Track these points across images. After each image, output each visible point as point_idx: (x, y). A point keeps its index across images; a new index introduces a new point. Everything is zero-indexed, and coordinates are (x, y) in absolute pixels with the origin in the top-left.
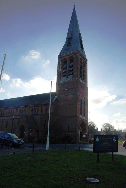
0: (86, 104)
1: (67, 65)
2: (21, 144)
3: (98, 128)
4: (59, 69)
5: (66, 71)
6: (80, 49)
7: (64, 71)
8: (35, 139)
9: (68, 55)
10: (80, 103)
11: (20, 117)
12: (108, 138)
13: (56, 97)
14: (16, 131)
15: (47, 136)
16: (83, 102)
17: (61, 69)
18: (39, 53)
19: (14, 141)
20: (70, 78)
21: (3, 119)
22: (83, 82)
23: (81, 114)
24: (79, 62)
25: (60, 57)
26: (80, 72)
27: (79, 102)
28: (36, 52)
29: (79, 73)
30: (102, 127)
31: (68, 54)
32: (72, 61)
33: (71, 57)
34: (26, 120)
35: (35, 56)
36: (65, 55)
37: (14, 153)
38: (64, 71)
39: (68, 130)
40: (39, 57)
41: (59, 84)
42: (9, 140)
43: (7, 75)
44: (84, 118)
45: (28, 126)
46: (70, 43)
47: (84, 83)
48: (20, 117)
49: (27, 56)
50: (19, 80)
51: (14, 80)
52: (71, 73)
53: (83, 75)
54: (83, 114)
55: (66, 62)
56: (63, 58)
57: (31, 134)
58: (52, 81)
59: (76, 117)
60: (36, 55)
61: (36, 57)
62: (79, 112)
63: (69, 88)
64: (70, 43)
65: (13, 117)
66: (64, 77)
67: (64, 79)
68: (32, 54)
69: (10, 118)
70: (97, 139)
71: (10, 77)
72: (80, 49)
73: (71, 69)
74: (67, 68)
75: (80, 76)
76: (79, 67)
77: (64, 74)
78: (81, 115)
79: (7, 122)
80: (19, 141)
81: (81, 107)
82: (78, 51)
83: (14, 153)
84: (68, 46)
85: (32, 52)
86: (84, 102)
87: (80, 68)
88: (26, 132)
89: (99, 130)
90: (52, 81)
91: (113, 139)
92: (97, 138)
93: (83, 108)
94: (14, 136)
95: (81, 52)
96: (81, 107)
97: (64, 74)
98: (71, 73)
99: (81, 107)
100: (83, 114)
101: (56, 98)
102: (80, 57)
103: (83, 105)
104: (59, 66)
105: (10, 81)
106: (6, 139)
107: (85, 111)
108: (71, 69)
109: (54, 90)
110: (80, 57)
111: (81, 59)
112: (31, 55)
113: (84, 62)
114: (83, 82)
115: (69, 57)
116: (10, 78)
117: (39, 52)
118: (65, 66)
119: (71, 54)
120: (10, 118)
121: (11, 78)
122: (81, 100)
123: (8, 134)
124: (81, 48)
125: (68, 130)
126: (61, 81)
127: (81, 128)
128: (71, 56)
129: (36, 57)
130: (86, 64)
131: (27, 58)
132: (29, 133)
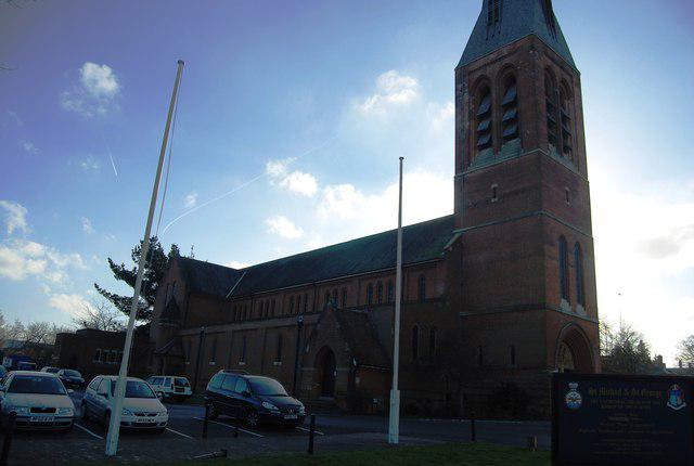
0: (585, 254)
1: (494, 102)
2: (295, 417)
3: (660, 358)
4: (463, 121)
5: (490, 125)
6: (541, 29)
7: (484, 125)
8: (375, 401)
9: (493, 62)
10: (555, 251)
11: (317, 316)
12: (635, 392)
13: (458, 232)
14: (305, 369)
15: (390, 387)
16: (571, 247)
17: (470, 119)
18: (413, 82)
19: (267, 405)
20: (509, 151)
21: (267, 328)
22: (564, 161)
23: (565, 295)
24: (540, 84)
25: (462, 73)
26: (550, 124)
27: (552, 244)
28: (402, 80)
29: (545, 129)
30: (679, 353)
31: (492, 56)
32: (511, 81)
33: (508, 66)
34: (338, 327)
35: (399, 92)
36: (481, 62)
37: (226, 452)
38: (484, 125)
39: (513, 363)
40: (413, 93)
41: (465, 183)
42: (248, 400)
43: (307, 176)
44: (581, 311)
45: (347, 349)
46: (497, 15)
47: (570, 166)
48: (317, 316)
49: (372, 97)
50: (346, 190)
51: (329, 192)
52: (511, 130)
53: (566, 134)
54: (573, 296)
55: (486, 92)
56: (476, 76)
57: (358, 381)
58: (401, 159)
59: (542, 306)
60: (404, 87)
61: (401, 98)
62: (554, 286)
63: (507, 191)
64: (497, 15)
65: (301, 318)
66: (485, 152)
67: (483, 161)
68: (387, 90)
69: (289, 322)
70: (574, 398)
71: (318, 182)
72: (541, 29)
73: (510, 114)
74: (494, 114)
75: (551, 139)
76: (543, 101)
77: (484, 140)
78: (564, 301)
79: (280, 337)
80: (285, 408)
81: (564, 264)
82: (533, 38)
83: (226, 452)
84: (490, 24)
85: (389, 79)
86: (578, 245)
87: (549, 107)
88: (340, 372)
89: (670, 363)
90: (401, 159)
91: (668, 398)
92: (569, 389)
93: (572, 271)
94: (276, 386)
95: (550, 41)
96: (562, 266)
97: (484, 140)
98: (511, 130)
99: (564, 264)
100: (573, 296)
101: (457, 236)
102: (542, 61)
103: (571, 258)
104: (462, 109)
105: (320, 197)
106: (239, 397)
107: (583, 289)
108: (510, 114)
109: (452, 212)
110: (542, 61)
111: (548, 69)
112: (385, 94)
113: (563, 81)
114: (564, 161)
115: (497, 67)
116: (319, 186)
117: (412, 77)
118: (483, 109)
119: (505, 57)
120: (289, 322)
121: (322, 184)
122: (562, 238)
123: (247, 380)
124: (545, 28)
125: (513, 363)
126: (470, 169)
127: (568, 355)
128: (507, 61)
129: (401, 98)
130: (576, 89)
131: (369, 105)
132: (351, 377)
